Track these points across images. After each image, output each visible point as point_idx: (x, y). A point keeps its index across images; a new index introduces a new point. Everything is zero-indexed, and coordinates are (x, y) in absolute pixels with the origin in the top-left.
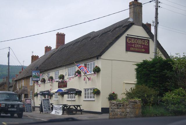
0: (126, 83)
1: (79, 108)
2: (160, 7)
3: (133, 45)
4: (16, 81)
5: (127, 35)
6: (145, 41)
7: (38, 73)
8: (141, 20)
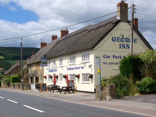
0: (114, 69)
2: (135, 12)
4: (28, 65)
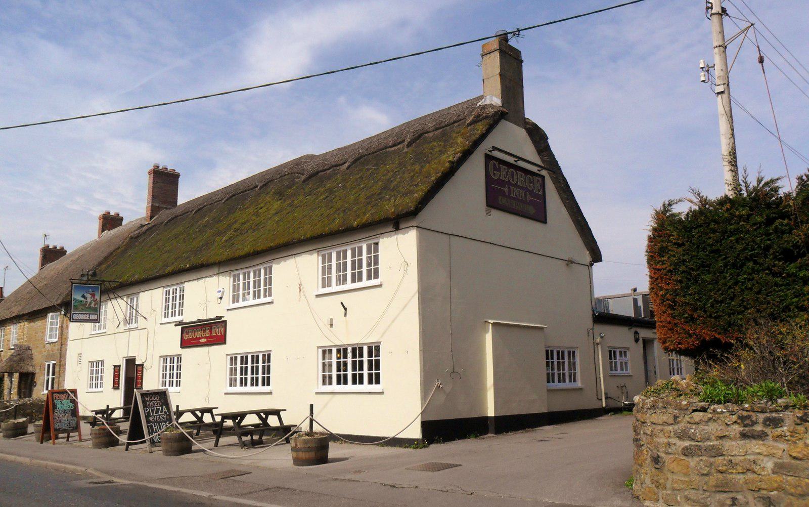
1: (207, 418)
3: (506, 189)
5: (494, 148)
6: (533, 178)
7: (93, 295)
8: (522, 106)
